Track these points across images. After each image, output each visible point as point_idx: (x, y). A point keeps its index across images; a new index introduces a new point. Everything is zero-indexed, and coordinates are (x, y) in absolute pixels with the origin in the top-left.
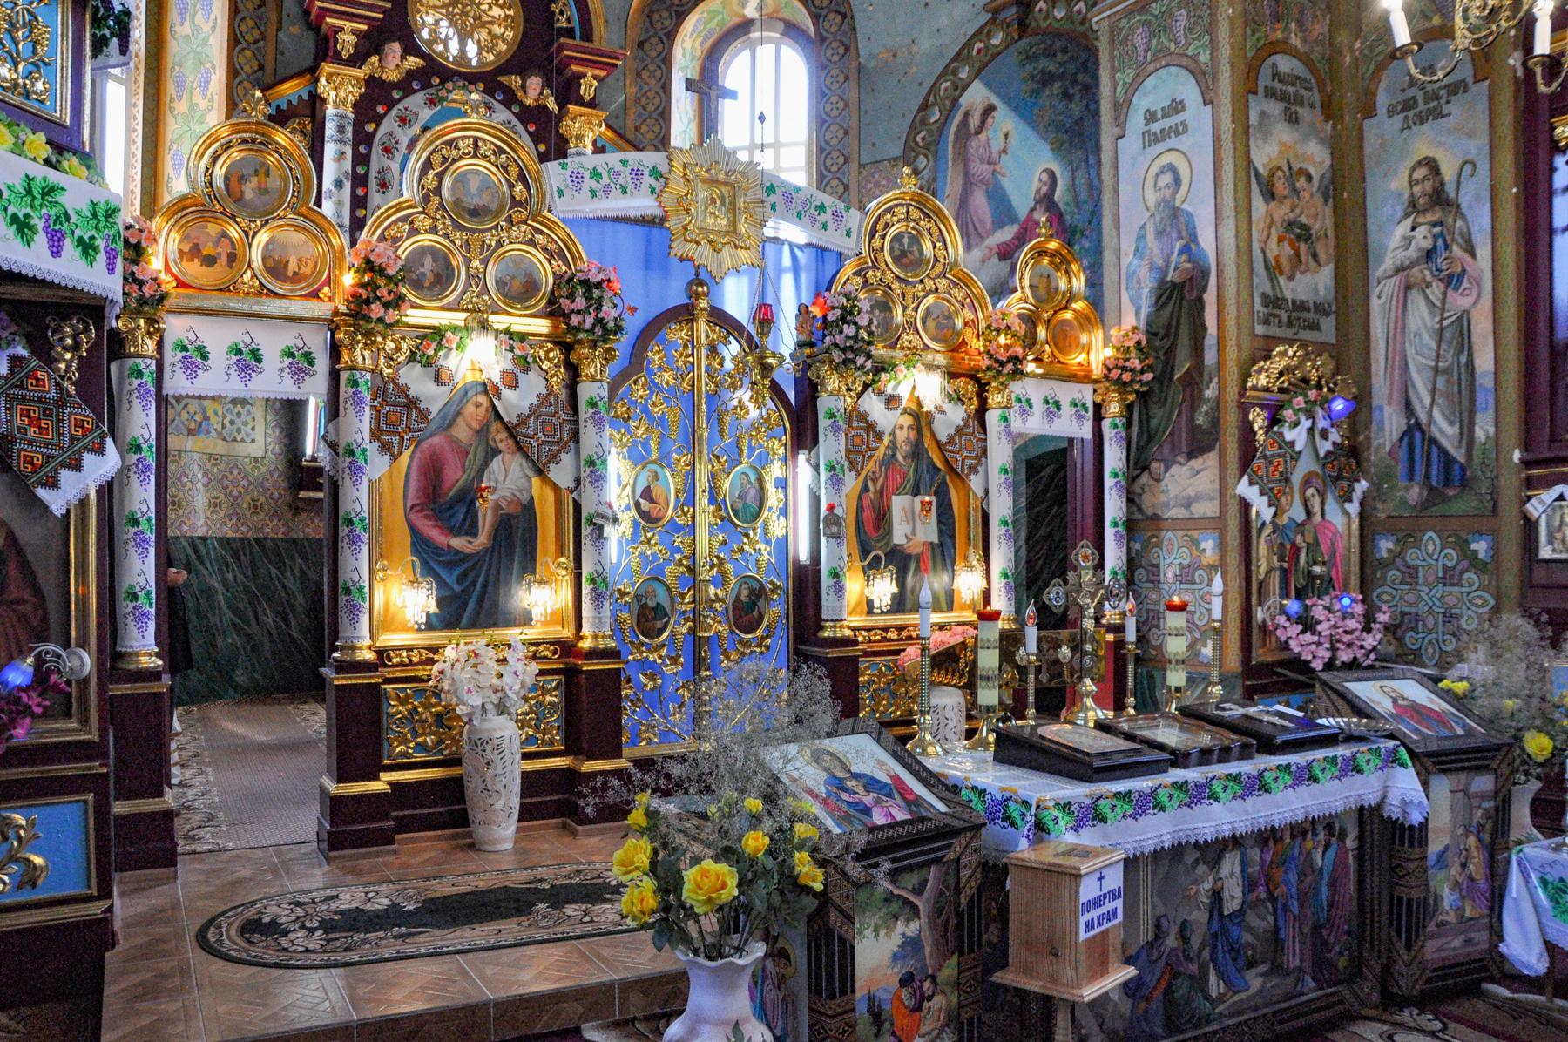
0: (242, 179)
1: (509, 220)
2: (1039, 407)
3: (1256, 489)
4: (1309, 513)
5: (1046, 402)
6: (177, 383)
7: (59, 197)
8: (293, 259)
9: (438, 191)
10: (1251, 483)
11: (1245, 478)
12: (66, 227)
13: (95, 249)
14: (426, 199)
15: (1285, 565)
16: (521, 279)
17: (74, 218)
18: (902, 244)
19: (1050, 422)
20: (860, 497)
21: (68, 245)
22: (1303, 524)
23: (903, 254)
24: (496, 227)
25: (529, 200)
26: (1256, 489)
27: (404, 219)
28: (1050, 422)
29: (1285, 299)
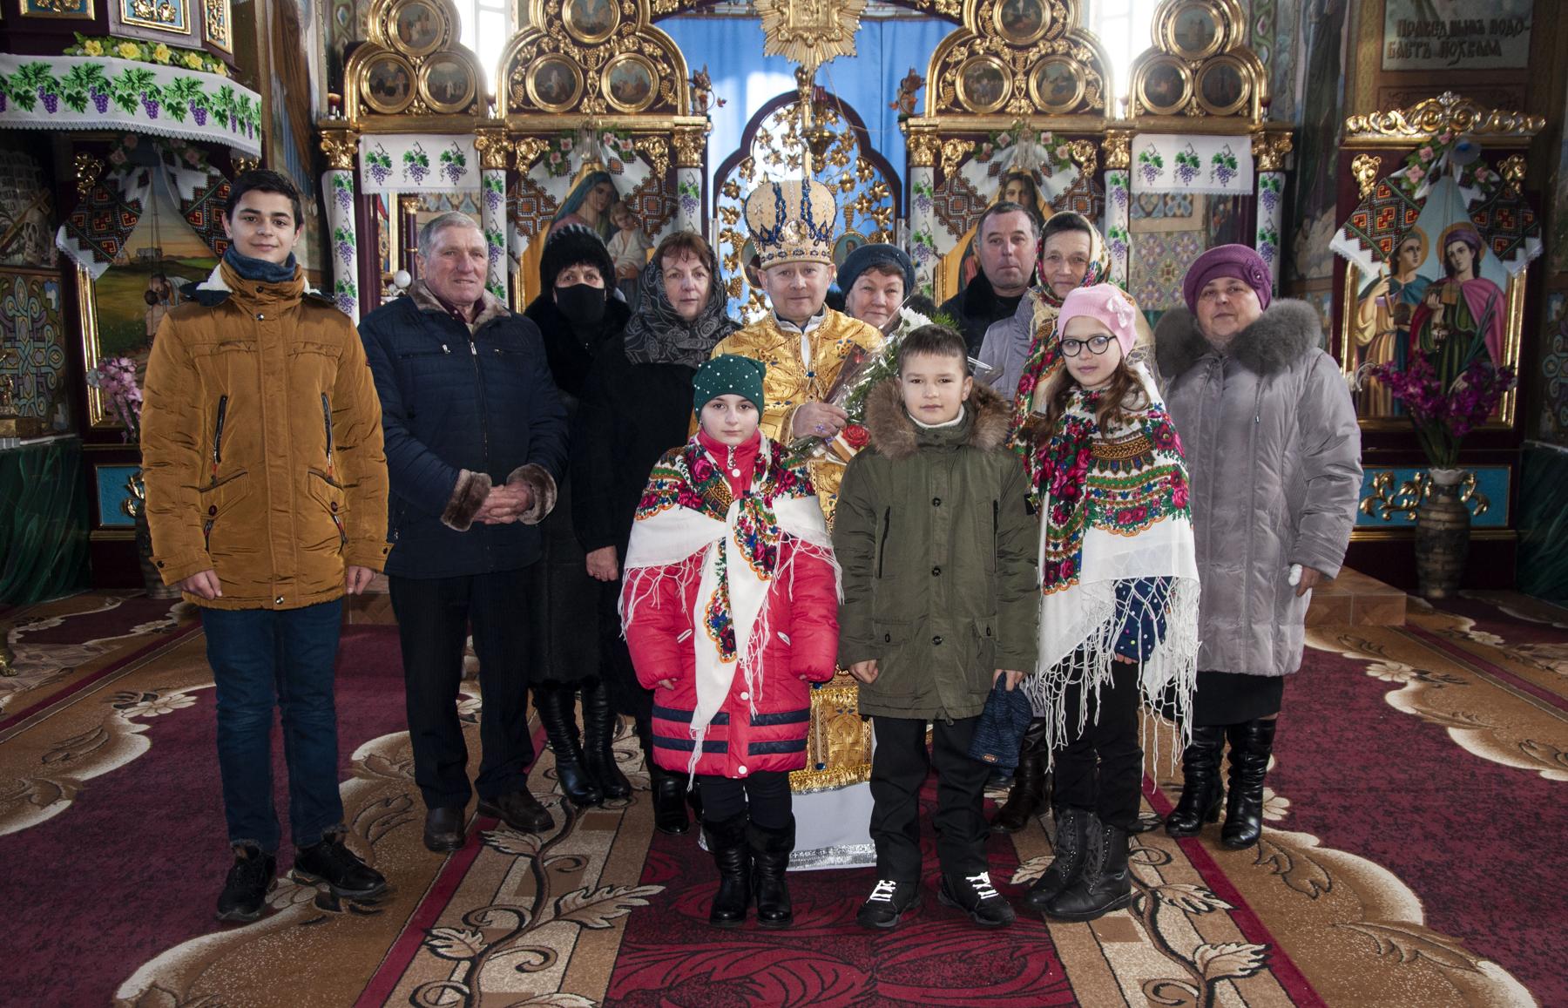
0: (410, 25)
1: (619, 33)
2: (1170, 165)
3: (1355, 243)
4: (1451, 270)
5: (1181, 159)
6: (370, 186)
7: (153, 81)
8: (450, 84)
9: (559, 16)
10: (1348, 237)
11: (1341, 232)
12: (158, 98)
13: (183, 111)
14: (550, 24)
15: (1407, 328)
16: (632, 83)
17: (164, 92)
18: (1016, 9)
19: (418, 179)
20: (963, 260)
21: (161, 110)
22: (1440, 283)
23: (1018, 18)
24: (608, 41)
25: (636, 13)
26: (1355, 243)
27: (532, 43)
28: (418, 179)
29: (1439, 23)
